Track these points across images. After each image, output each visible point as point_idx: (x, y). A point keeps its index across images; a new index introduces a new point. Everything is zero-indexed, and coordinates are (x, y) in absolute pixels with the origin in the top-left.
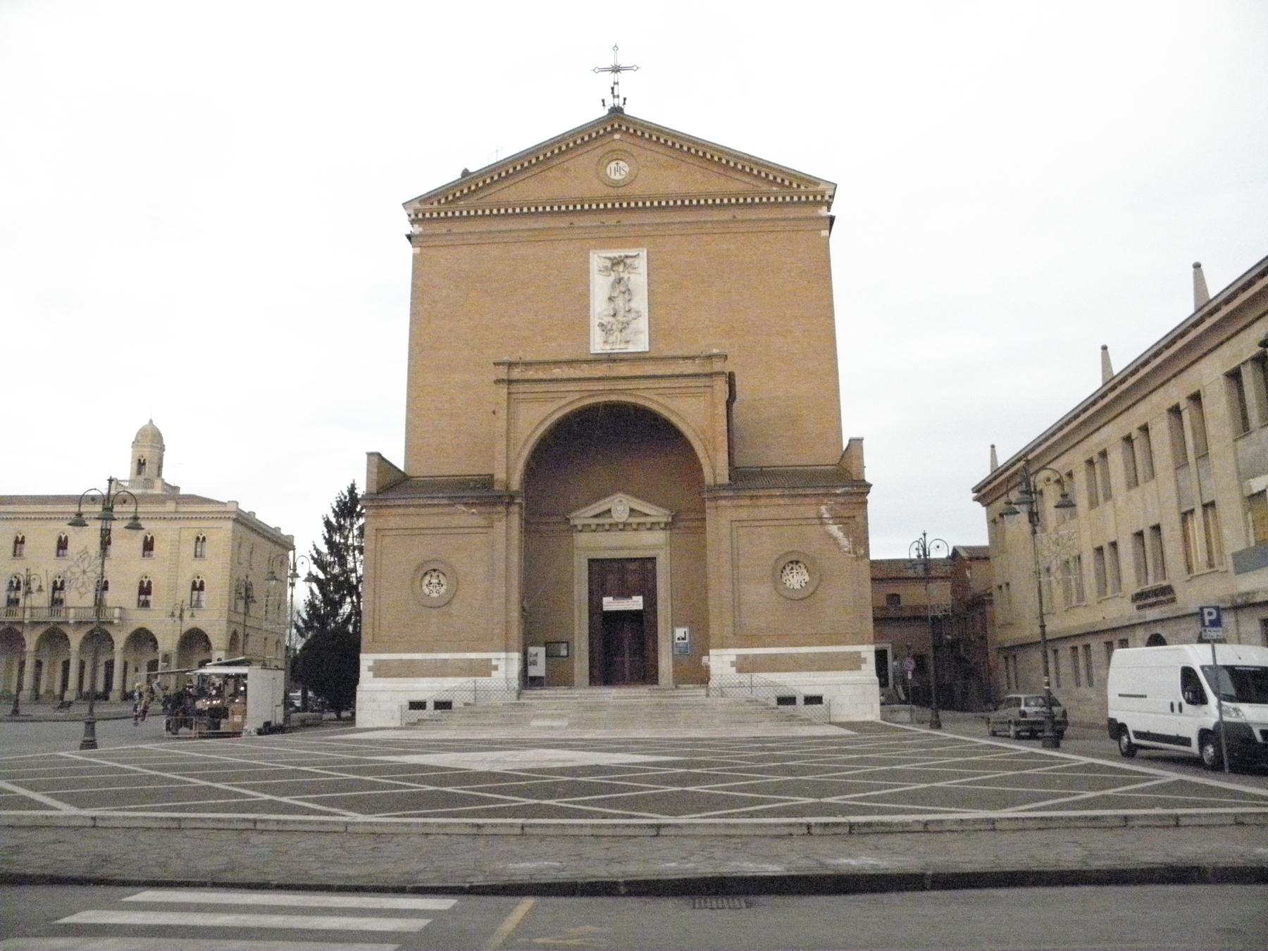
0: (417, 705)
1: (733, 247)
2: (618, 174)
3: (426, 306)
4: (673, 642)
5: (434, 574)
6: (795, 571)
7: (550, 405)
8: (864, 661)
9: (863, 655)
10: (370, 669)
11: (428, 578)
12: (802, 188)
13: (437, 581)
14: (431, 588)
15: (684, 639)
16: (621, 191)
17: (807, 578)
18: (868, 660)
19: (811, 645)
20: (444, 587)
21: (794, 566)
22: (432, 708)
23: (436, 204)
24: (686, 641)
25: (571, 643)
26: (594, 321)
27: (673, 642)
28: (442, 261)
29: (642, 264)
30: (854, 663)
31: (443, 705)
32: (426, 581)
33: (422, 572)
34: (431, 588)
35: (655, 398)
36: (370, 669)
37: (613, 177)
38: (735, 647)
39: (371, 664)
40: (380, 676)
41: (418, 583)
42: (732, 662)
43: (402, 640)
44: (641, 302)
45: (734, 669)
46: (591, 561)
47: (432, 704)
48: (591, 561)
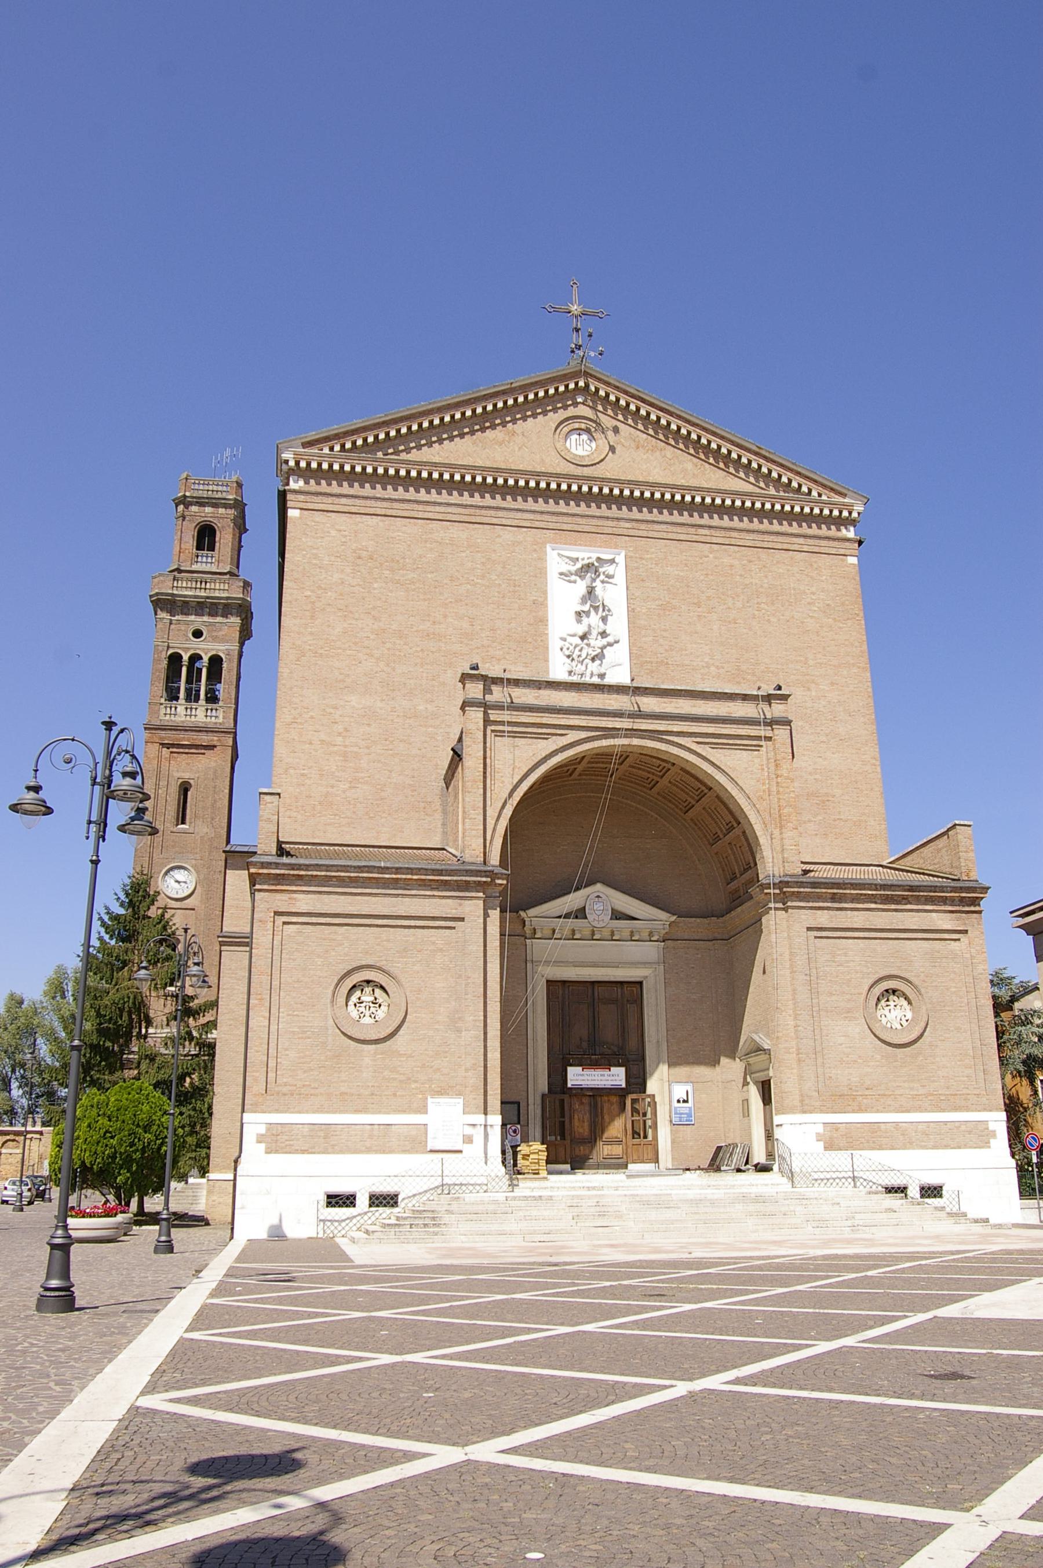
0: (338, 1200)
1: (736, 563)
2: (580, 448)
3: (308, 593)
4: (670, 1106)
5: (368, 990)
6: (891, 1003)
7: (542, 743)
8: (993, 1134)
9: (992, 1126)
10: (260, 1139)
11: (358, 993)
12: (824, 497)
13: (372, 999)
14: (362, 1009)
15: (685, 1101)
16: (587, 472)
17: (909, 1015)
18: (998, 1133)
19: (920, 1109)
20: (384, 1008)
21: (891, 997)
22: (918, 1195)
23: (326, 451)
24: (690, 1104)
25: (523, 1105)
26: (554, 644)
27: (670, 1106)
28: (333, 533)
29: (619, 572)
30: (981, 1137)
31: (383, 1200)
32: (354, 999)
33: (349, 983)
34: (362, 1009)
35: (694, 747)
36: (260, 1139)
37: (573, 450)
38: (822, 1112)
39: (262, 1129)
40: (276, 1152)
41: (342, 1000)
42: (818, 1134)
43: (317, 1091)
44: (618, 626)
45: (821, 1144)
46: (550, 983)
47: (358, 1202)
48: (550, 983)
